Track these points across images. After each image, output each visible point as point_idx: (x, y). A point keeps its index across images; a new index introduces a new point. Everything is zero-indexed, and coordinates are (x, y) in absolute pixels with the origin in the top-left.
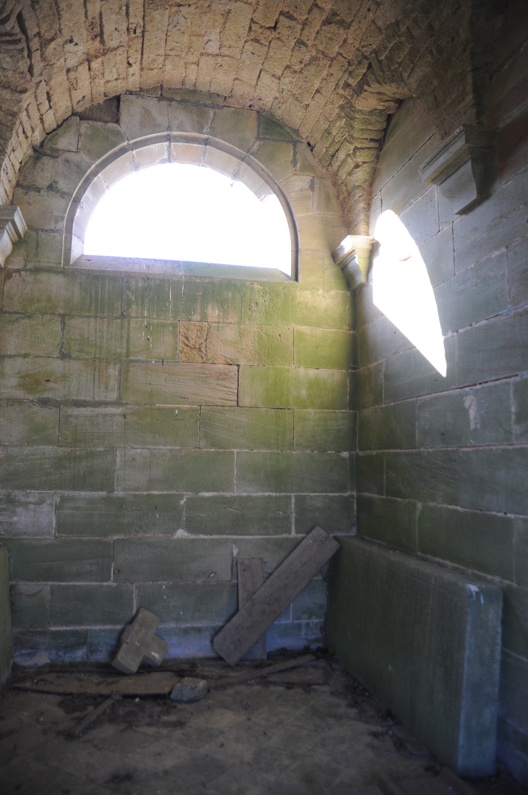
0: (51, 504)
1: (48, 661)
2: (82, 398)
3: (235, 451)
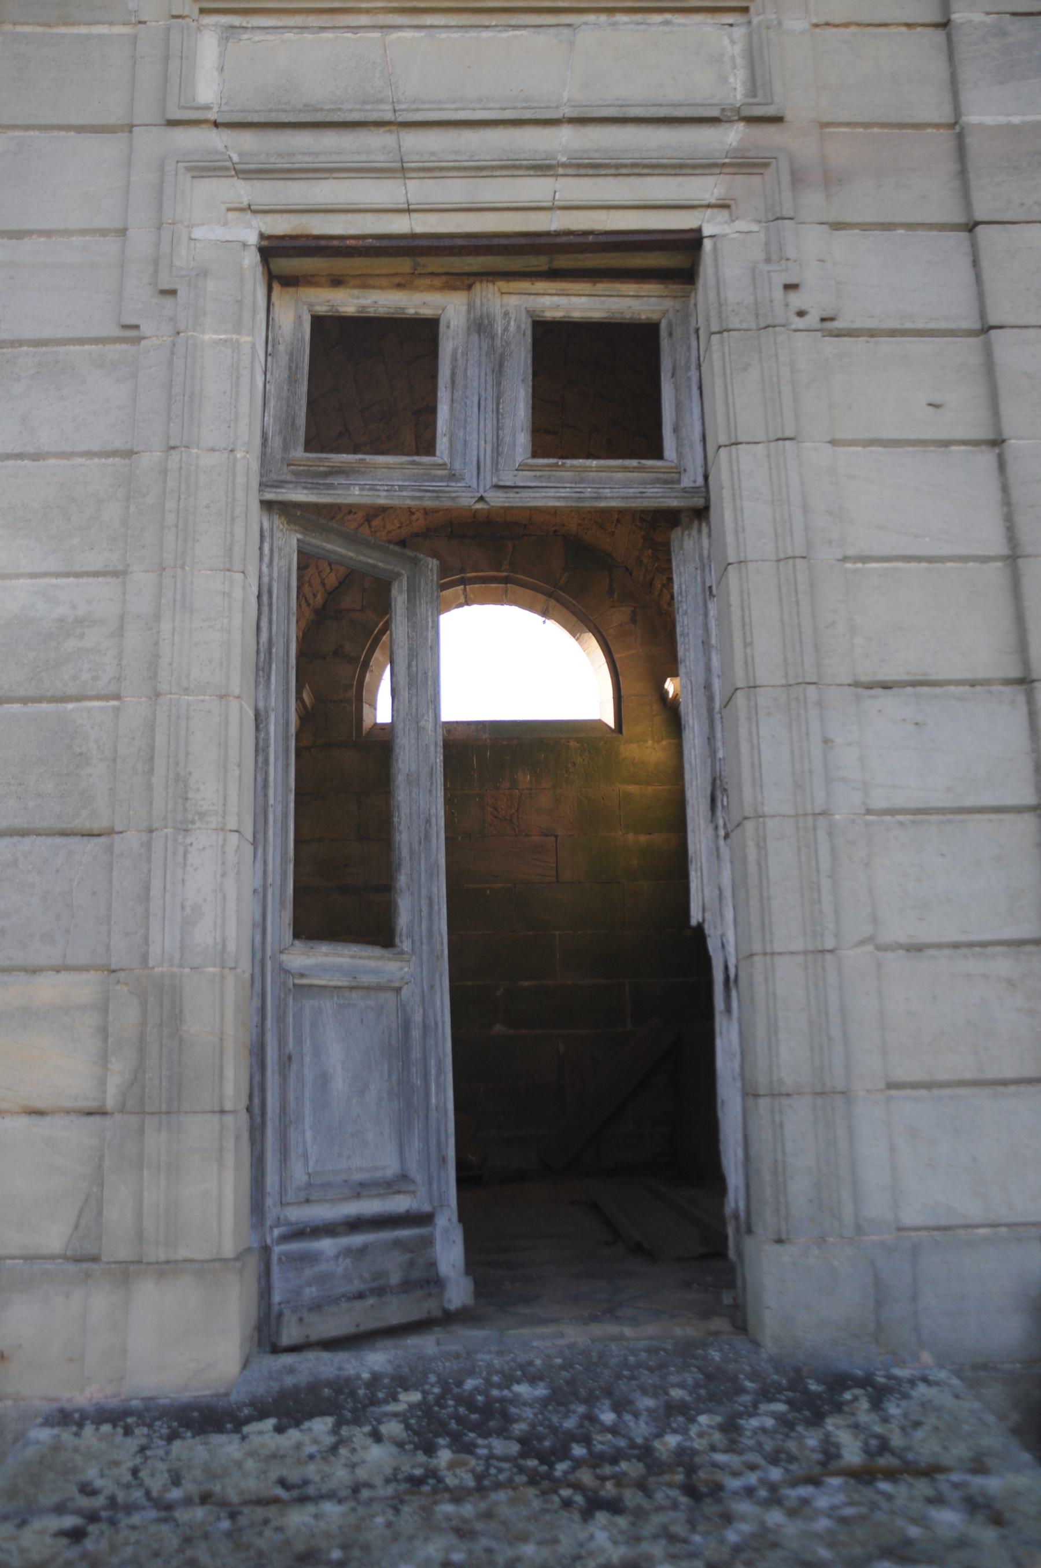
3: (557, 933)
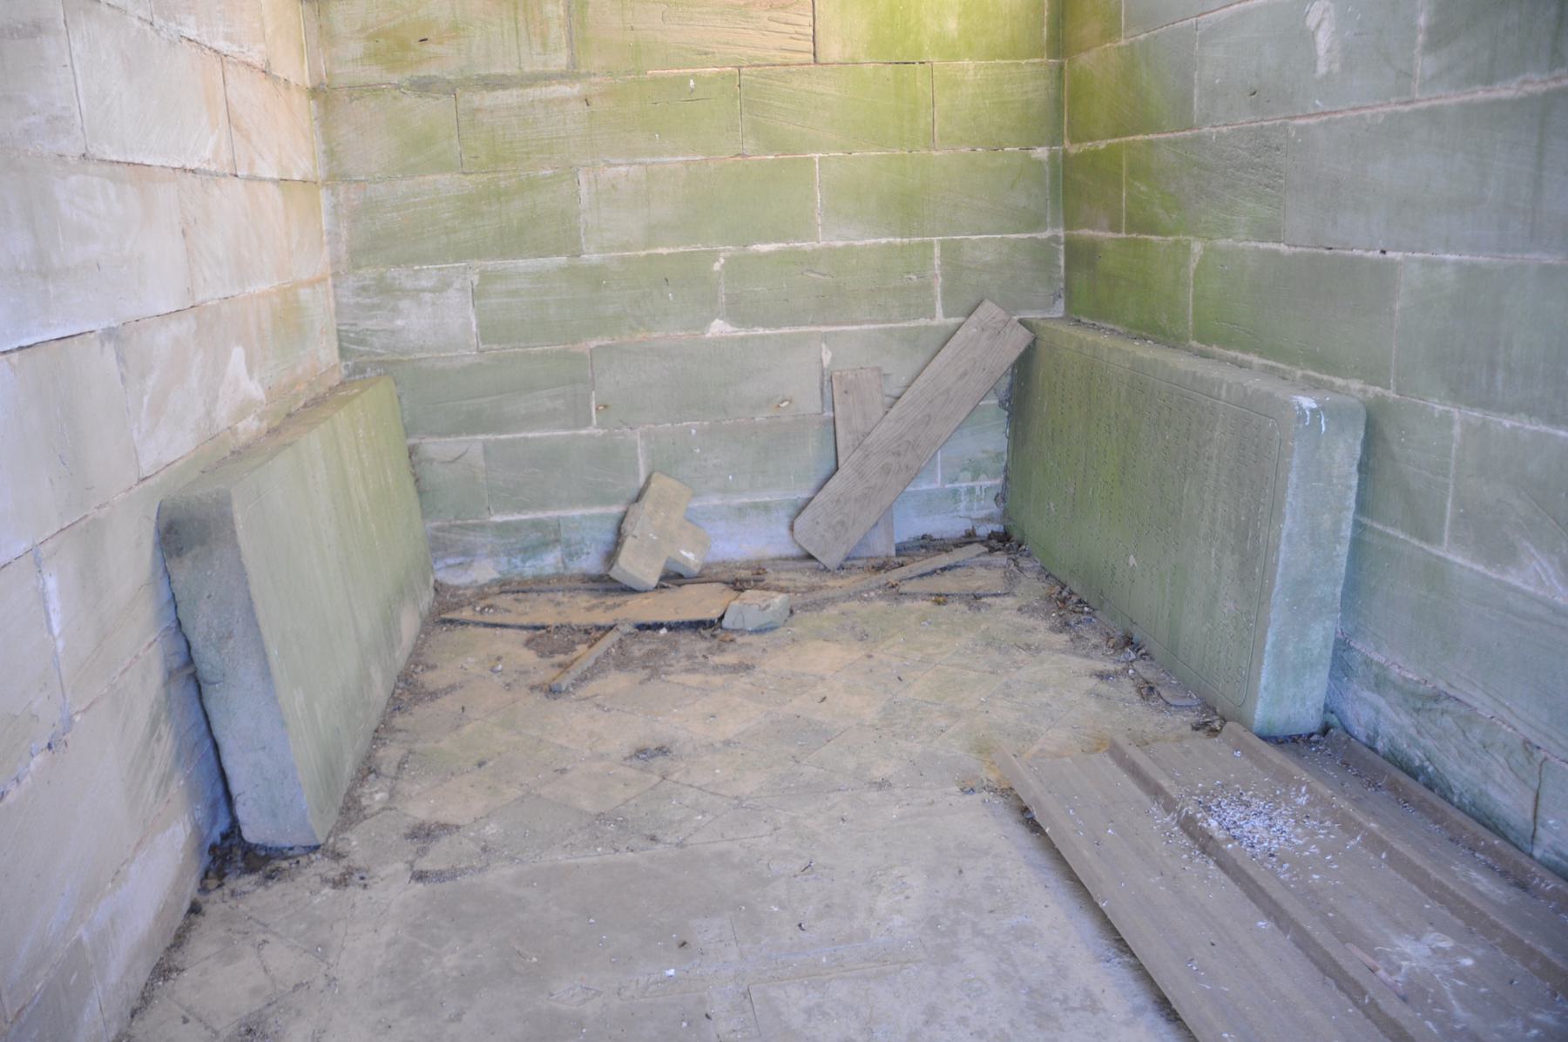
0: (463, 289)
1: (496, 575)
2: (497, 70)
3: (817, 156)
